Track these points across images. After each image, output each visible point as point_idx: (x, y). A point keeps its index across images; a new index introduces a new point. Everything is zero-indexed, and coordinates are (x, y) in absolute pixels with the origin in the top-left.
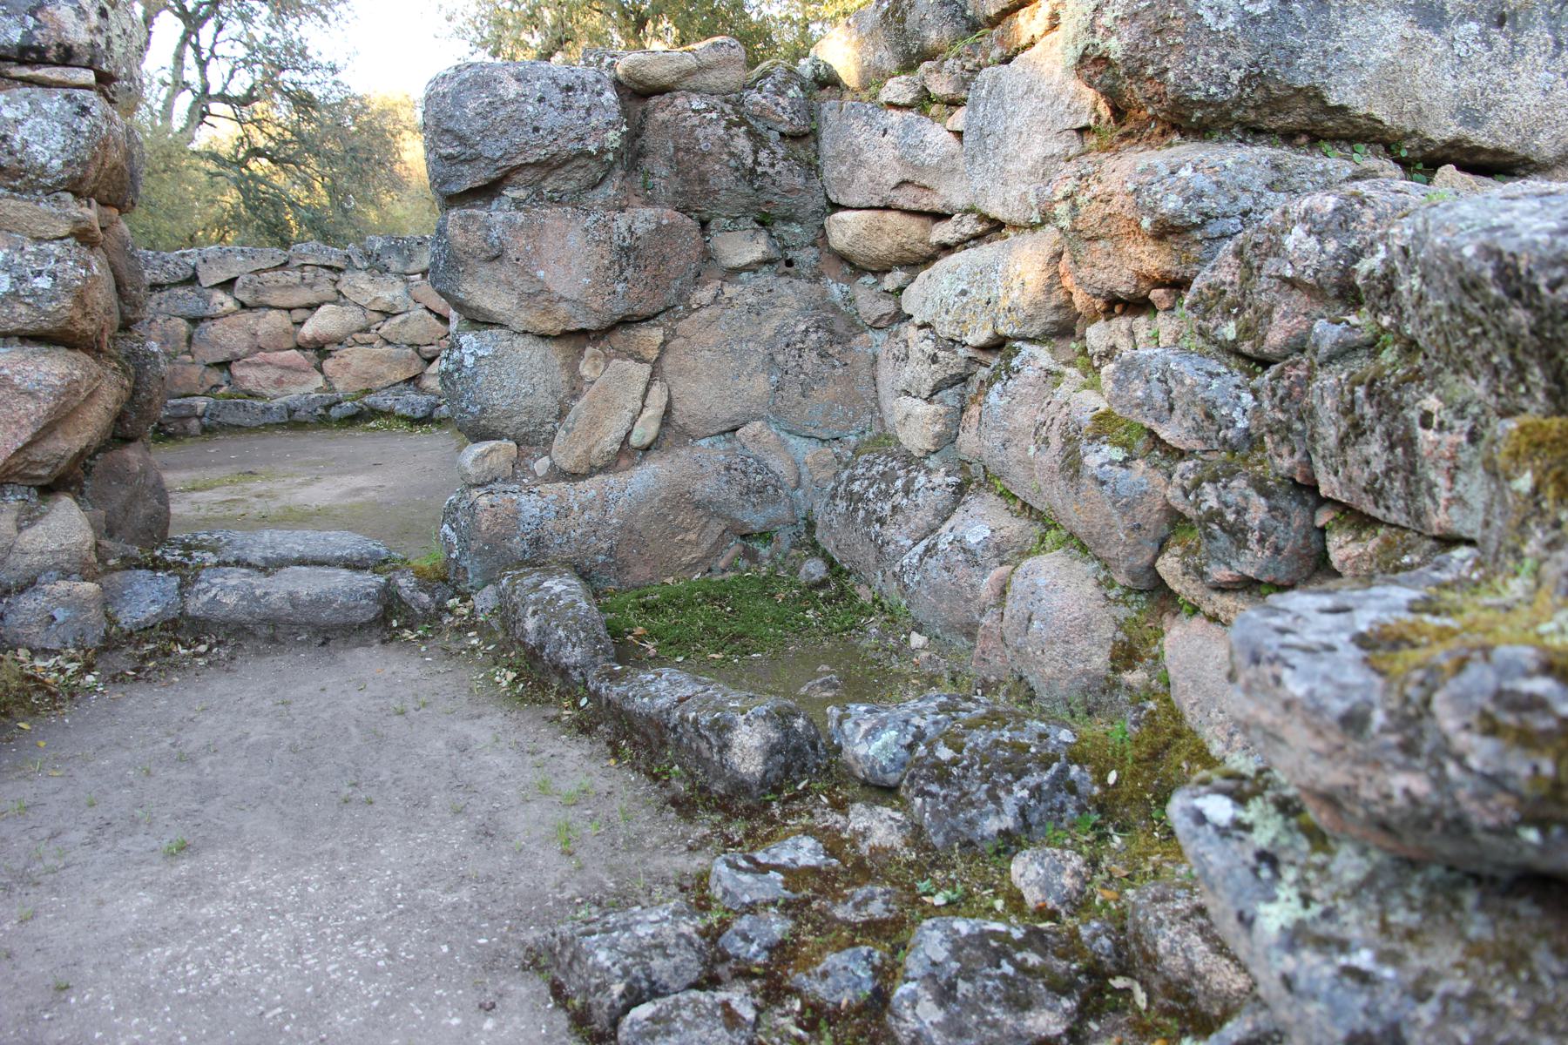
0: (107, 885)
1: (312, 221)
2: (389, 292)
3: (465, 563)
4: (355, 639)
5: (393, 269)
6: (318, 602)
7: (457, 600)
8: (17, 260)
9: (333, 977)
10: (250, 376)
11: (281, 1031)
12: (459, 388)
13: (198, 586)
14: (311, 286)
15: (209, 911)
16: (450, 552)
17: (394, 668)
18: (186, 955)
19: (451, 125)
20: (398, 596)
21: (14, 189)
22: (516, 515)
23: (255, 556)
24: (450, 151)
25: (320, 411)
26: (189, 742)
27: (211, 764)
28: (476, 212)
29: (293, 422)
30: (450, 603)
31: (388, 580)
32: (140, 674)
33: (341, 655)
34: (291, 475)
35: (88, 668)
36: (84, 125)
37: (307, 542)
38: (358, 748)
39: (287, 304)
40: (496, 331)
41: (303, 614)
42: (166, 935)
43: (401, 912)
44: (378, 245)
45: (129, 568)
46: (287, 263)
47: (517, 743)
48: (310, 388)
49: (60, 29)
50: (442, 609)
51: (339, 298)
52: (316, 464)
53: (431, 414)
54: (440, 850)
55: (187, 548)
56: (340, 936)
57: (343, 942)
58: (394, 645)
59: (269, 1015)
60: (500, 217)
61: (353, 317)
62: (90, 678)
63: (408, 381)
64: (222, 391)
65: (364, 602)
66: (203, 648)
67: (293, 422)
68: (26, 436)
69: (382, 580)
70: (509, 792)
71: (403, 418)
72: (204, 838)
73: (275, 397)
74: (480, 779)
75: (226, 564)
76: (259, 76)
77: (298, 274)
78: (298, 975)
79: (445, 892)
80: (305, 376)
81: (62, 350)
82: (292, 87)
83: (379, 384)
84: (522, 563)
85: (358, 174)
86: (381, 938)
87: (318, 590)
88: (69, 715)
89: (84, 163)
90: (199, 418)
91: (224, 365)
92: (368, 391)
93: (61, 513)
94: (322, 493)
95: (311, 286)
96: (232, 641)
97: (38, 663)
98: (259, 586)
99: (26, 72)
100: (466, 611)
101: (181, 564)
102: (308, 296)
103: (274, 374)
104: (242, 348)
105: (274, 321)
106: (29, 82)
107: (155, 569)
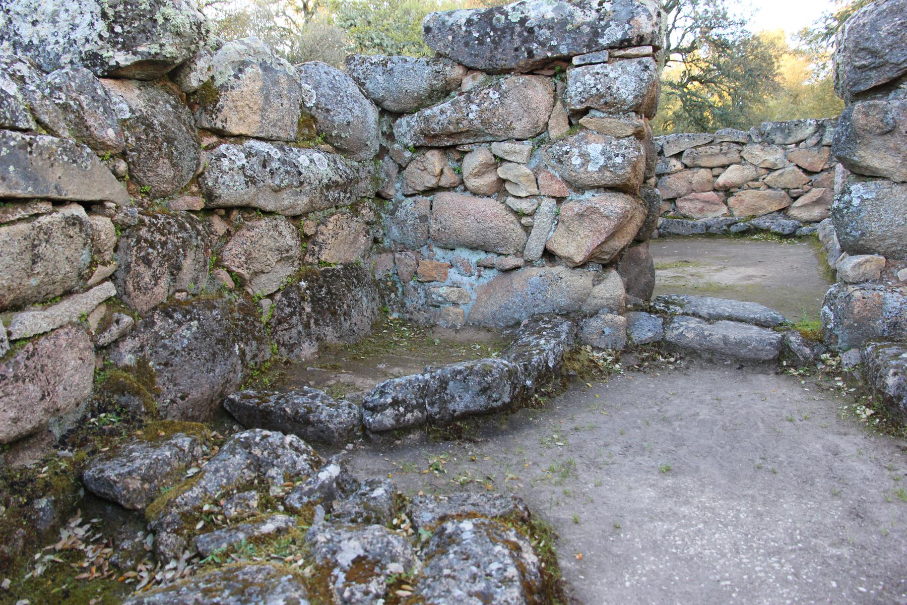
0: (632, 479)
1: (721, 115)
2: (774, 156)
3: (837, 333)
4: (759, 369)
5: (777, 142)
6: (739, 344)
7: (828, 355)
8: (608, 149)
9: (759, 574)
10: (685, 206)
11: (730, 596)
12: (846, 219)
13: (672, 325)
14: (725, 154)
15: (685, 510)
16: (826, 324)
17: (784, 391)
18: (675, 531)
19: (867, 45)
20: (789, 347)
21: (610, 113)
22: (881, 305)
23: (704, 311)
24: (864, 62)
25: (725, 228)
26: (667, 411)
27: (679, 426)
28: (877, 102)
29: (708, 233)
30: (823, 356)
31: (784, 336)
32: (640, 369)
33: (750, 377)
34: (709, 264)
35: (617, 361)
36: (645, 76)
37: (733, 307)
38: (764, 436)
39: (710, 165)
40: (879, 182)
41: (730, 349)
42: (662, 517)
43: (801, 549)
44: (769, 128)
45: (637, 310)
46: (713, 141)
47: (877, 459)
48: (719, 214)
49: (640, 27)
50: (817, 359)
51: (742, 161)
52: (722, 259)
53: (794, 232)
54: (824, 517)
55: (667, 303)
56: (762, 551)
57: (764, 555)
58: (783, 376)
59: (723, 583)
60: (897, 103)
61: (748, 172)
62: (617, 366)
63: (779, 211)
64: (670, 214)
65: (768, 348)
66: (672, 360)
67: (708, 233)
68: (602, 239)
69: (779, 336)
70: (873, 491)
71: (776, 234)
72: (679, 467)
73: (699, 218)
74: (850, 476)
75: (687, 314)
76: (698, 35)
77: (719, 147)
78: (738, 565)
79: (830, 545)
80: (717, 207)
81: (622, 194)
82: (716, 38)
83: (761, 212)
84: (882, 338)
85: (752, 86)
86: (790, 561)
87: (740, 337)
88: (608, 384)
89: (643, 96)
90: (658, 229)
91: (672, 200)
92: (753, 217)
93: (612, 278)
94: (729, 276)
95: (725, 154)
96: (688, 358)
97: (595, 354)
98: (706, 330)
99: (622, 52)
100: (834, 363)
101: (663, 311)
102: (723, 160)
103: (699, 205)
104: (683, 191)
105: (704, 174)
106: (622, 57)
107: (650, 312)
